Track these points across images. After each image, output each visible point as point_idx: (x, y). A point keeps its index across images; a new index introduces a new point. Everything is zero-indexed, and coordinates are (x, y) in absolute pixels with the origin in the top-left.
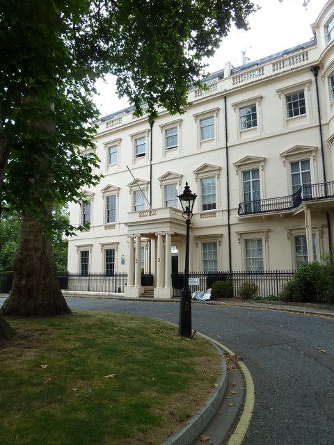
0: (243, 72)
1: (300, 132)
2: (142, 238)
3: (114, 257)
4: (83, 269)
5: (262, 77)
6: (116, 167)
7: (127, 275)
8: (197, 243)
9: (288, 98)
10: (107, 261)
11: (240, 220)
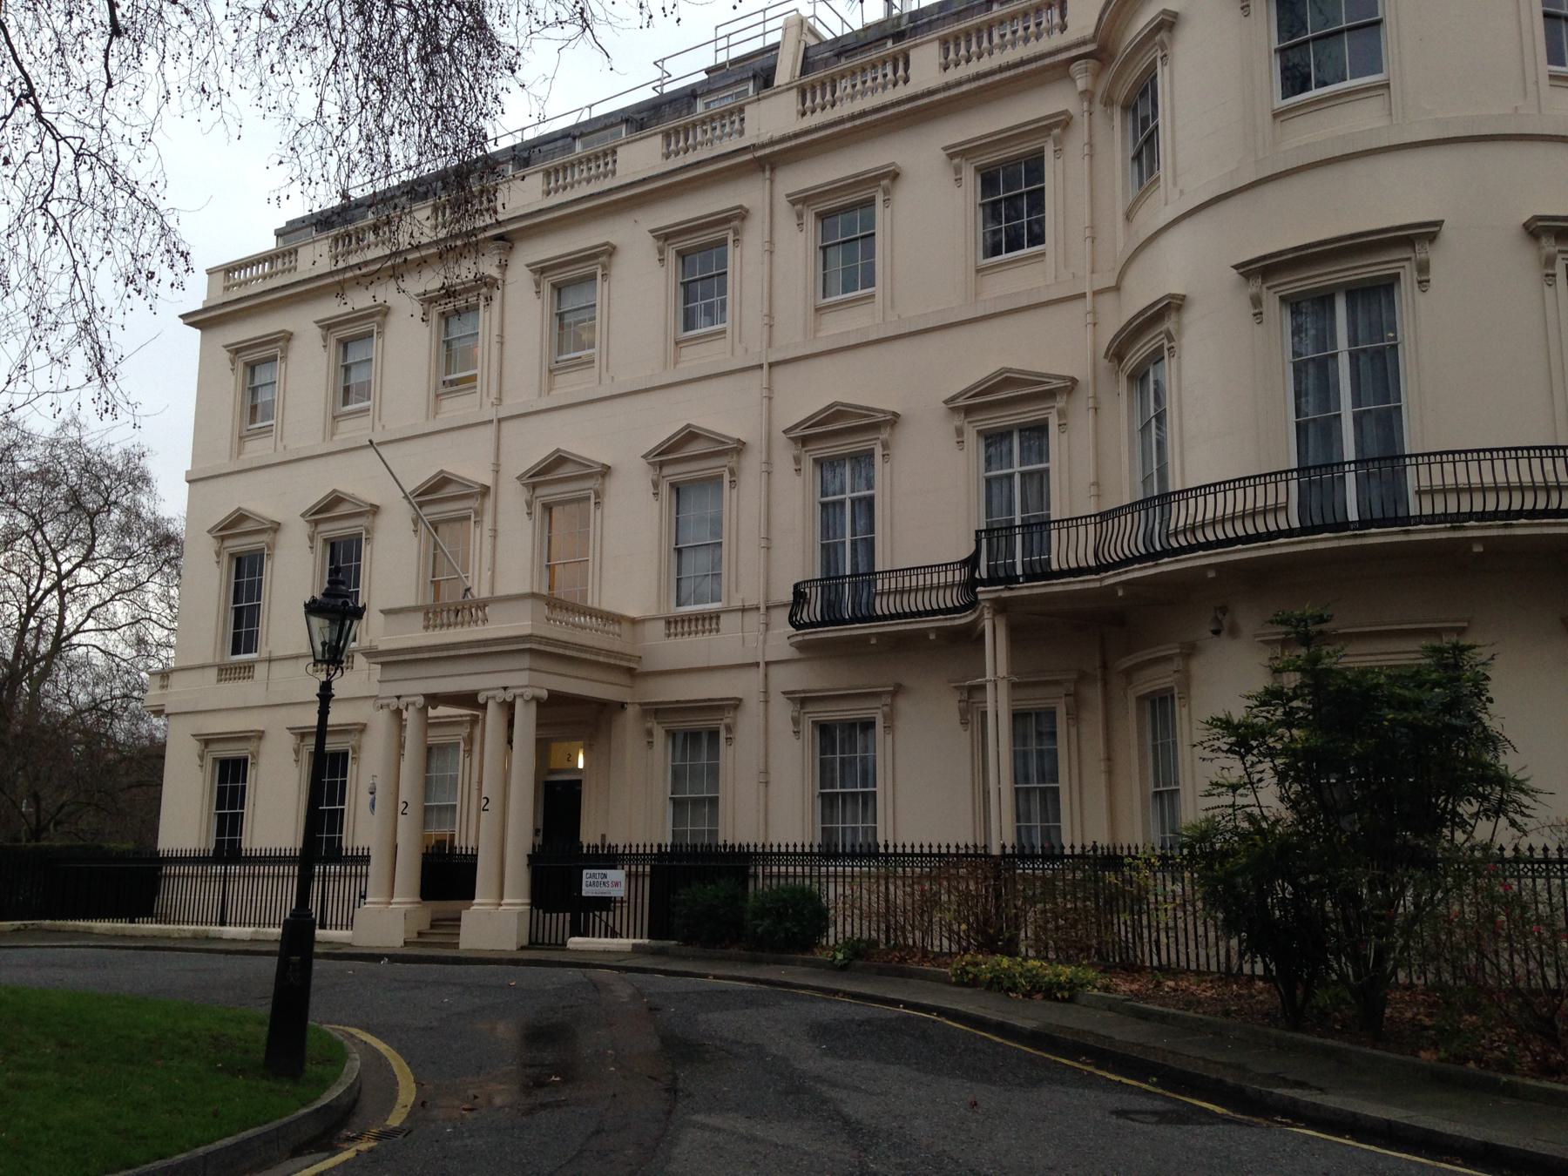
0: (844, 64)
1: (1042, 312)
2: (431, 712)
4: (220, 832)
5: (902, 91)
6: (365, 421)
8: (650, 733)
9: (989, 180)
10: (220, 806)
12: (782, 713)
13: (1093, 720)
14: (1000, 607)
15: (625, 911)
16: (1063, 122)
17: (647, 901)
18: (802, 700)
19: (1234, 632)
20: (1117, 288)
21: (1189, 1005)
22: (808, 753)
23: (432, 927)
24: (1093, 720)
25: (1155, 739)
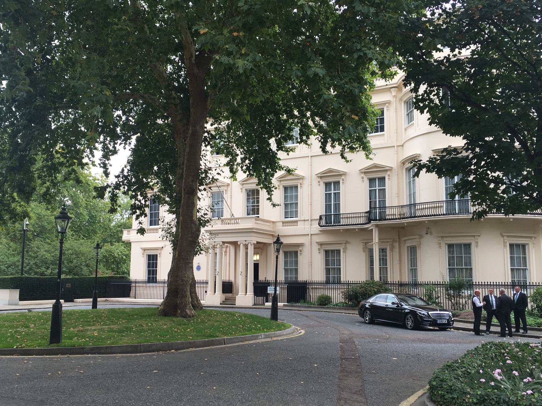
3: (156, 263)
10: (149, 267)
11: (320, 231)
12: (316, 247)
13: (396, 251)
14: (377, 226)
15: (422, 292)
16: (389, 102)
17: (286, 294)
19: (431, 234)
20: (402, 146)
22: (323, 256)
23: (225, 300)
24: (396, 251)
25: (411, 256)
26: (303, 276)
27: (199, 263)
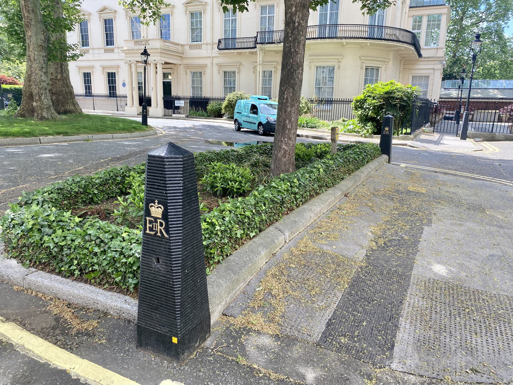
7: (126, 97)
8: (186, 72)
12: (215, 69)
18: (220, 66)
21: (102, 126)
26: (206, 93)
27: (124, 81)
